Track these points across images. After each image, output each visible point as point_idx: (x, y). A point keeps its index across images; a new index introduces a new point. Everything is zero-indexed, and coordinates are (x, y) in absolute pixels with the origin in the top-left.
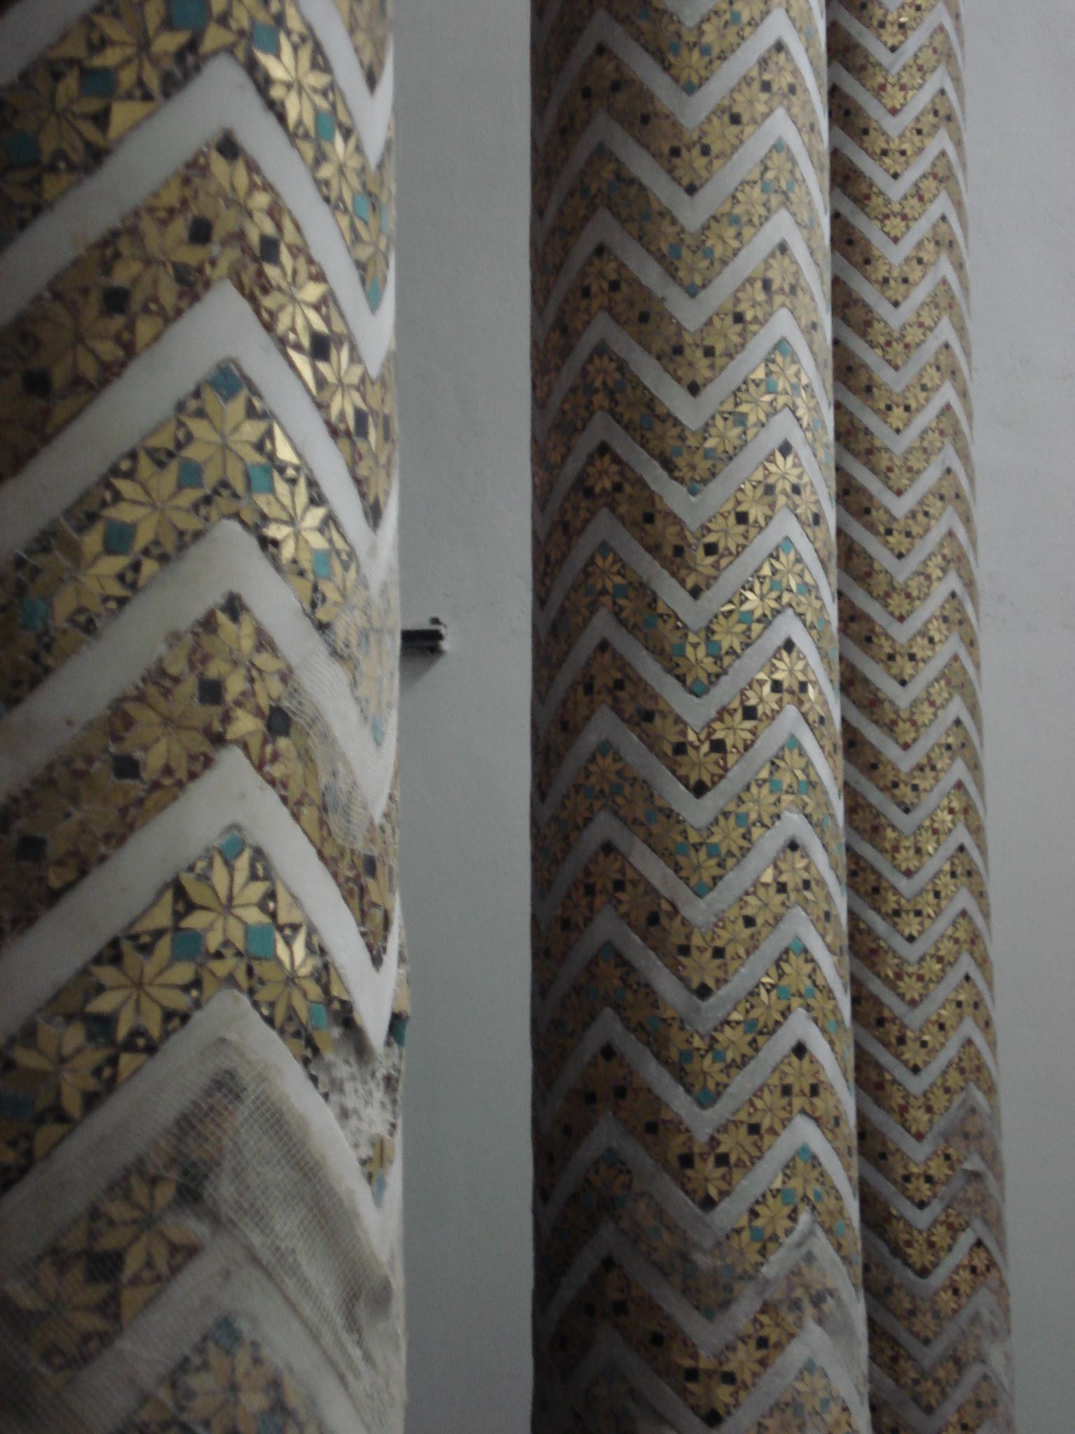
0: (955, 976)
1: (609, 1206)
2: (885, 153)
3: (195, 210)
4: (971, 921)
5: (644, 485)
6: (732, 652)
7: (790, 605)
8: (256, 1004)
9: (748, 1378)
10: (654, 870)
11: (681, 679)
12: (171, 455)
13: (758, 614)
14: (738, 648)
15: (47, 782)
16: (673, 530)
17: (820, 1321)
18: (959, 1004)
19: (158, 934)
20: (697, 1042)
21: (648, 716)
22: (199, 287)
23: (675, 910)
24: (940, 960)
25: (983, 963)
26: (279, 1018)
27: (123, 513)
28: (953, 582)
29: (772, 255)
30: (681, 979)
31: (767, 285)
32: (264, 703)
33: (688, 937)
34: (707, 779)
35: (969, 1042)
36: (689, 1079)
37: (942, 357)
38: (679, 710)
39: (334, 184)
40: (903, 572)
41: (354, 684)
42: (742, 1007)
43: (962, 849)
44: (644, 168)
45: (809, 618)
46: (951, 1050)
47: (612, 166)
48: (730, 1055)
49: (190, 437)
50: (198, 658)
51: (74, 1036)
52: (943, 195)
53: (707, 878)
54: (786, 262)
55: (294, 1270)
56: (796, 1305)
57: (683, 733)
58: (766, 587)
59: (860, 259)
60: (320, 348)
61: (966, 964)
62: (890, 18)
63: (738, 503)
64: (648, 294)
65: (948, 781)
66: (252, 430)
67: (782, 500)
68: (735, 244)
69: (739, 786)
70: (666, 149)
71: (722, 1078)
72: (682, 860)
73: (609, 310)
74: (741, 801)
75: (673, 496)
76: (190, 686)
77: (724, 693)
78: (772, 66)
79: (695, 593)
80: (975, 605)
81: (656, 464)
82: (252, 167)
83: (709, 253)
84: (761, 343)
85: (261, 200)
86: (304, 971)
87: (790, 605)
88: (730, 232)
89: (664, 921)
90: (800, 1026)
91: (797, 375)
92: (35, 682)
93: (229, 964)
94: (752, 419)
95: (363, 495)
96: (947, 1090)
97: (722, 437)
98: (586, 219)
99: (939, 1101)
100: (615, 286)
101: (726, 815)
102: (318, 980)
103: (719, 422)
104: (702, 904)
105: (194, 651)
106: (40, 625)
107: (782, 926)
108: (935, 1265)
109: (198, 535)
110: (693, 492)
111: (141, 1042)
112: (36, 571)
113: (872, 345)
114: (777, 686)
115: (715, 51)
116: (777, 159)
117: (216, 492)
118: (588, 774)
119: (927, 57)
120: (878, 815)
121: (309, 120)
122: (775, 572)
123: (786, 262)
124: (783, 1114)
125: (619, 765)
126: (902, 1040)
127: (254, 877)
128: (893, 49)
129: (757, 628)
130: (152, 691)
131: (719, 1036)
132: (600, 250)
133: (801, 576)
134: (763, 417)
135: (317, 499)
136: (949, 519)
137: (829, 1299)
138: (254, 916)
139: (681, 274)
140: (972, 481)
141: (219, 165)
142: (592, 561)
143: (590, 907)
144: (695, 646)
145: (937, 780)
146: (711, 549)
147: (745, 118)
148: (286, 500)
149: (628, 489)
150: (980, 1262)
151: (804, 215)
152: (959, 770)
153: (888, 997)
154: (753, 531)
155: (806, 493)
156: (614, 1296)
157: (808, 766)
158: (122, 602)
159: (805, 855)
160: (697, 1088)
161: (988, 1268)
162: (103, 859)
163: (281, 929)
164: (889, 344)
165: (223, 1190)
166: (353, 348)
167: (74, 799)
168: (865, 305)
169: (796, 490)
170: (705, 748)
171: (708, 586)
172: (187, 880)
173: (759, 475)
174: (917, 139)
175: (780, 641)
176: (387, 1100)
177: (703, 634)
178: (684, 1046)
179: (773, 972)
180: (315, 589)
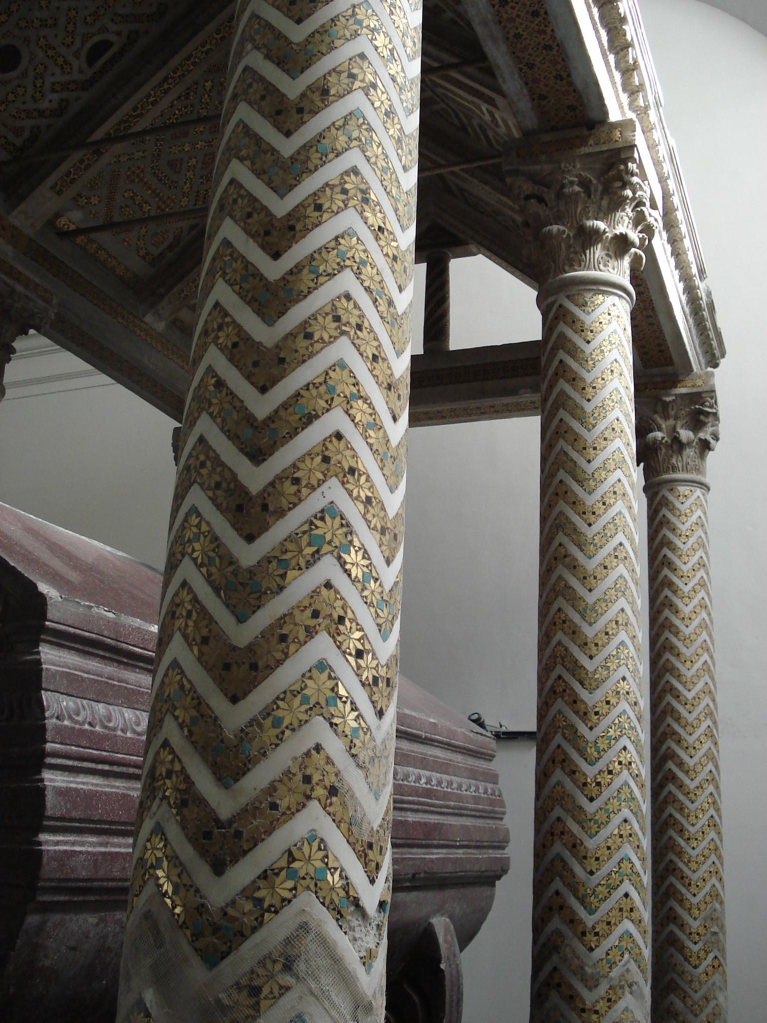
0: (709, 862)
1: (556, 949)
2: (682, 577)
3: (314, 607)
4: (715, 842)
5: (574, 691)
6: (604, 750)
7: (625, 734)
8: (317, 897)
9: (603, 1012)
10: (575, 828)
11: (586, 759)
12: (299, 693)
13: (613, 737)
14: (606, 749)
15: (244, 810)
16: (583, 706)
17: (631, 993)
18: (710, 872)
19: (282, 869)
20: (589, 891)
21: (574, 772)
22: (313, 634)
23: (582, 843)
24: (704, 856)
25: (720, 857)
26: (327, 902)
27: (279, 713)
28: (709, 722)
29: (619, 613)
30: (584, 868)
31: (617, 622)
32: (328, 784)
33: (586, 853)
34: (594, 796)
35: (714, 885)
36: (585, 905)
37: (703, 645)
38: (585, 770)
39: (369, 597)
40: (691, 718)
41: (367, 777)
42: (605, 879)
43: (712, 816)
44: (574, 582)
45: (632, 739)
46: (707, 889)
47: (564, 582)
48: (600, 896)
49: (306, 686)
50: (303, 767)
51: (248, 906)
52: (703, 591)
53: (593, 832)
54: (624, 615)
55: (329, 998)
56: (622, 987)
57: (586, 779)
58: (616, 727)
59: (674, 611)
60: (359, 654)
61: (713, 858)
62: (683, 533)
63: (607, 697)
64: (576, 625)
65: (707, 792)
66: (330, 684)
67: (622, 697)
68: (606, 609)
69: (606, 798)
70: (582, 577)
71: (598, 905)
72: (584, 825)
73: (562, 630)
74: (607, 804)
75: (583, 694)
76: (300, 776)
77: (601, 765)
78: (618, 551)
79: (591, 728)
80: (717, 730)
81: (577, 683)
82: (337, 592)
83: (596, 611)
84: (615, 642)
85: (339, 603)
86: (339, 885)
87: (625, 734)
88: (604, 605)
89: (578, 846)
90: (627, 887)
91: (628, 653)
92: (244, 774)
93: (308, 881)
94: (611, 668)
95: (375, 707)
96: (706, 903)
97: (601, 674)
98: (555, 599)
99: (703, 906)
100: (564, 622)
101: (601, 809)
102: (344, 889)
103: (600, 669)
104: (592, 841)
105: (302, 764)
106: (247, 753)
107: (621, 850)
108: (700, 965)
109: (306, 721)
110: (591, 693)
111: (273, 909)
112: (247, 733)
113: (679, 640)
114: (620, 763)
115: (599, 546)
116: (620, 581)
117: (314, 706)
118: (553, 792)
119: (696, 546)
120: (682, 804)
121: (360, 576)
122: (620, 722)
123: (624, 615)
124: (620, 919)
125: (563, 790)
126: (690, 884)
127: (320, 849)
128: (684, 543)
129: (613, 742)
130: (285, 779)
131: (597, 889)
132: (560, 610)
133: (630, 724)
134: (615, 668)
135: (354, 708)
136: (707, 700)
137: (635, 986)
138: (319, 864)
139: (586, 618)
140: (715, 687)
141: (324, 591)
142: (555, 716)
143: (552, 840)
144: (591, 748)
145: (703, 792)
146: (597, 713)
147: (609, 567)
148: (342, 710)
149: (568, 691)
150: (716, 964)
151: (630, 599)
152: (711, 788)
153: (685, 869)
154: (612, 707)
155: (631, 695)
156: (557, 981)
157: (631, 792)
158: (277, 745)
159: (630, 824)
160: (588, 908)
161: (719, 966)
162: (263, 840)
163: (330, 869)
164: (685, 640)
165: (301, 967)
166: (374, 654)
167: (254, 818)
168: (676, 627)
169: (628, 693)
170: (594, 784)
171: (596, 726)
172: (294, 849)
173: (614, 688)
174: (693, 572)
175: (622, 747)
176: (377, 934)
177: (594, 743)
178: (584, 892)
179: (617, 866)
180: (352, 742)
